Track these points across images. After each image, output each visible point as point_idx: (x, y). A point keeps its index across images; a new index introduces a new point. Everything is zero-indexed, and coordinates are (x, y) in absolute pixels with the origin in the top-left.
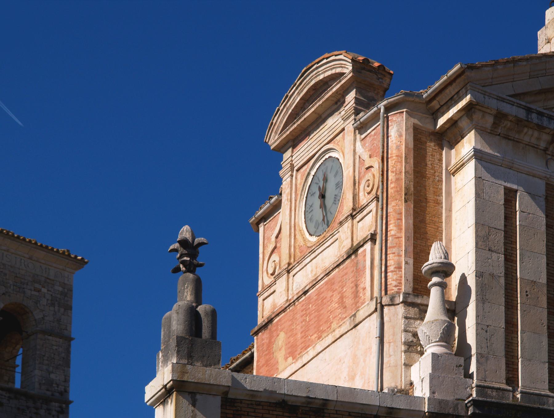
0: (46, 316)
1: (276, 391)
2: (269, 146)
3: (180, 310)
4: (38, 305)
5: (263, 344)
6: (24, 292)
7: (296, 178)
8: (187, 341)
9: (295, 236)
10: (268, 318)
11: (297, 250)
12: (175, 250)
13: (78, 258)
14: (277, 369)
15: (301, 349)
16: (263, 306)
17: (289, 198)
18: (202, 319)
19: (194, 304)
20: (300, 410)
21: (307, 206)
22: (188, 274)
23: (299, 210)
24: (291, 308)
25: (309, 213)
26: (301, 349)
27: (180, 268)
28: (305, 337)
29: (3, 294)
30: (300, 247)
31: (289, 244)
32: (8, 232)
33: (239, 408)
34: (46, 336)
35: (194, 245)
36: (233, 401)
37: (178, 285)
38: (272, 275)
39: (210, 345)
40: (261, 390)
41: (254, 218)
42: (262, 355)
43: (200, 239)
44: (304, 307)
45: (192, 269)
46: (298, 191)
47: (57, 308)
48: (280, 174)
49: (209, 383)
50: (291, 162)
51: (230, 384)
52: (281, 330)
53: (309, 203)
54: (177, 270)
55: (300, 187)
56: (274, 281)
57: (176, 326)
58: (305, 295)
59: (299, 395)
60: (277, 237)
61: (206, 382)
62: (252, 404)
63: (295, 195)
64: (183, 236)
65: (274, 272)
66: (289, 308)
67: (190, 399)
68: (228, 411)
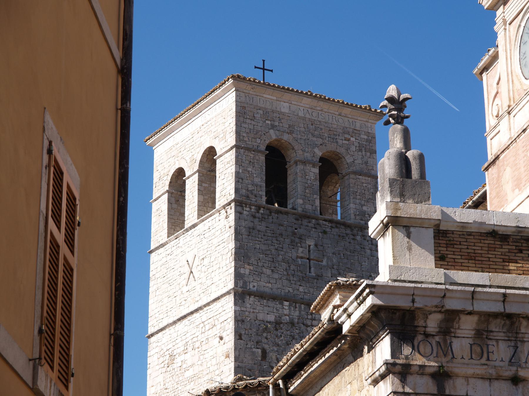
0: (356, 160)
1: (485, 223)
2: (483, 7)
3: (391, 156)
4: (349, 151)
5: (493, 178)
6: (337, 142)
7: (509, 31)
8: (399, 182)
9: (513, 81)
10: (495, 156)
11: (516, 94)
12: (385, 106)
13: (378, 111)
14: (507, 200)
15: (525, 181)
16: (491, 145)
17: (504, 48)
18: (411, 163)
19: (404, 151)
20: (511, 239)
21: (521, 54)
22: (396, 125)
23: (514, 58)
24: (513, 145)
25: (524, 60)
26: (525, 181)
27: (390, 121)
28: (527, 170)
29: (321, 145)
30: (518, 91)
31: (508, 89)
32: (321, 96)
33: (451, 238)
34: (357, 176)
35: (400, 101)
36: (445, 233)
37: (389, 135)
38: (497, 117)
39: (419, 184)
40: (471, 222)
41: (477, 70)
42: (493, 188)
43: (404, 95)
44: (524, 144)
45: (400, 120)
46: (512, 42)
47: (364, 152)
48: (495, 29)
49: (420, 217)
50: (503, 18)
51: (440, 218)
52: (507, 165)
53: (523, 51)
54: (387, 123)
55: (513, 38)
56: (498, 122)
57: (388, 170)
58: (524, 133)
59: (508, 225)
60: (498, 84)
61: (417, 217)
62: (463, 235)
63: (510, 45)
64: (390, 94)
65: (498, 114)
66: (512, 145)
67: (405, 232)
68: (440, 242)
